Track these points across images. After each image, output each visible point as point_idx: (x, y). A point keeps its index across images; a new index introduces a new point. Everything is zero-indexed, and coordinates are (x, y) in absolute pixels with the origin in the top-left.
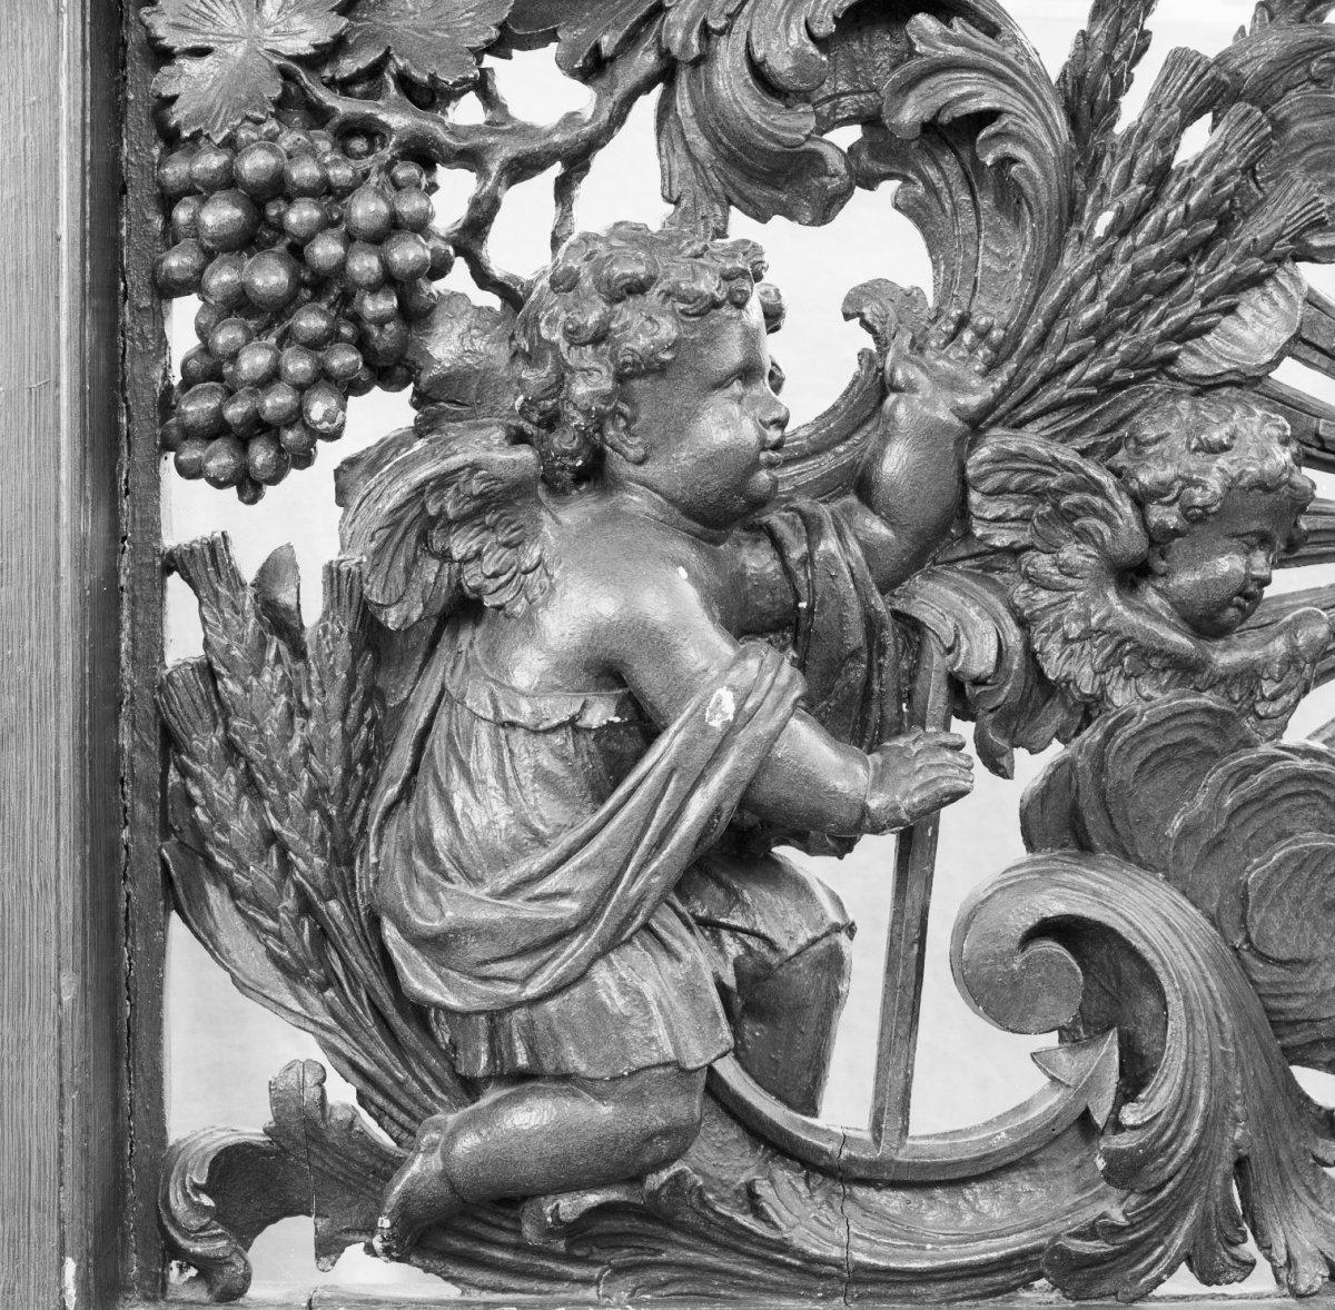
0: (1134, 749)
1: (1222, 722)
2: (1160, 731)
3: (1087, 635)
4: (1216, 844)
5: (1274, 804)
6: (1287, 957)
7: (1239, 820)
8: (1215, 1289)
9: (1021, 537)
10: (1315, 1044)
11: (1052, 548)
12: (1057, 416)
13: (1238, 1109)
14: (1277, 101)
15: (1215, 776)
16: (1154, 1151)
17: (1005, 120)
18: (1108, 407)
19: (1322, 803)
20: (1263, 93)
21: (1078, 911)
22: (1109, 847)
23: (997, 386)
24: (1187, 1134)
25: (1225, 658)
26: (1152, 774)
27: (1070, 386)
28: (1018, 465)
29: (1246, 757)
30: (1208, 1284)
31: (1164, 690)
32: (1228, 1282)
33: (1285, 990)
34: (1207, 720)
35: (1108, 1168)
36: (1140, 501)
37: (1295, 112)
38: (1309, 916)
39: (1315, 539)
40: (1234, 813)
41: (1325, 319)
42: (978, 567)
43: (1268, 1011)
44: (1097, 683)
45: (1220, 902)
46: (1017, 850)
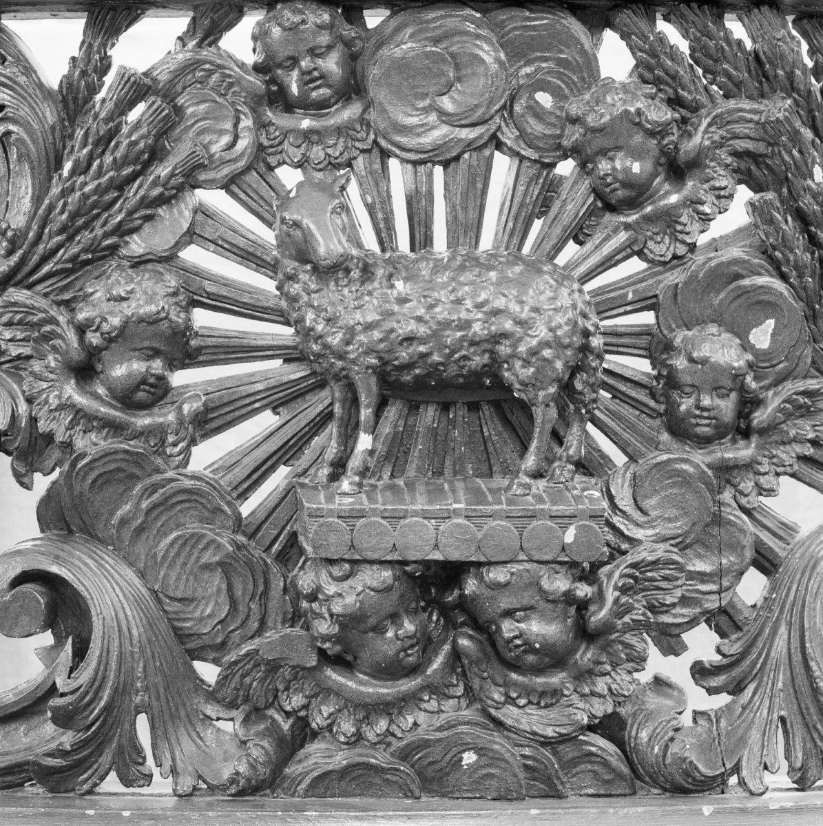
0: (86, 474)
1: (137, 459)
2: (100, 463)
3: (61, 407)
4: (140, 530)
5: (173, 506)
6: (180, 596)
7: (153, 515)
8: (131, 790)
9: (26, 351)
10: (203, 648)
11: (42, 357)
12: (50, 282)
13: (139, 685)
14: (179, 95)
15: (138, 488)
16: (79, 708)
17: (7, 110)
18: (82, 275)
19: (200, 507)
20: (169, 94)
21: (41, 567)
22: (81, 530)
23: (12, 263)
24: (101, 698)
25: (143, 421)
26: (100, 488)
27: (56, 264)
28: (16, 309)
29: (157, 478)
30: (128, 786)
31: (105, 439)
32: (139, 786)
33: (182, 616)
34: (127, 457)
35: (53, 716)
36: (81, 330)
37: (186, 101)
38: (191, 573)
39: (207, 351)
40: (149, 511)
41: (210, 222)
42: (12, 367)
43: (175, 629)
44: (67, 435)
45: (146, 563)
46: (33, 529)
